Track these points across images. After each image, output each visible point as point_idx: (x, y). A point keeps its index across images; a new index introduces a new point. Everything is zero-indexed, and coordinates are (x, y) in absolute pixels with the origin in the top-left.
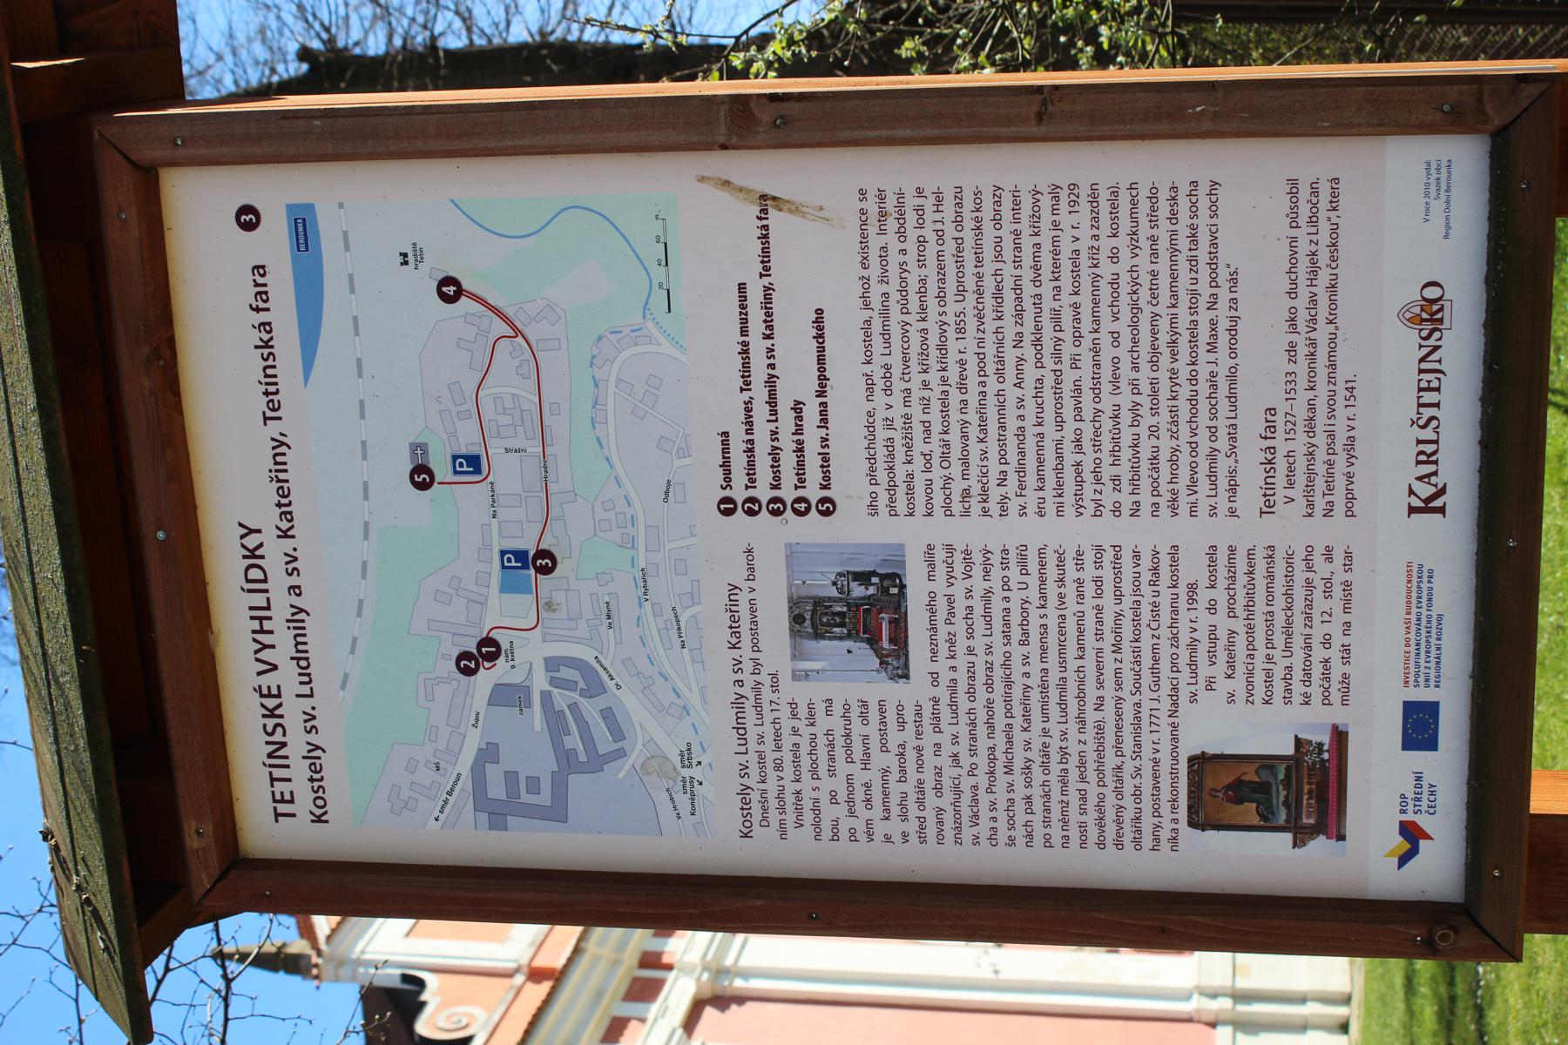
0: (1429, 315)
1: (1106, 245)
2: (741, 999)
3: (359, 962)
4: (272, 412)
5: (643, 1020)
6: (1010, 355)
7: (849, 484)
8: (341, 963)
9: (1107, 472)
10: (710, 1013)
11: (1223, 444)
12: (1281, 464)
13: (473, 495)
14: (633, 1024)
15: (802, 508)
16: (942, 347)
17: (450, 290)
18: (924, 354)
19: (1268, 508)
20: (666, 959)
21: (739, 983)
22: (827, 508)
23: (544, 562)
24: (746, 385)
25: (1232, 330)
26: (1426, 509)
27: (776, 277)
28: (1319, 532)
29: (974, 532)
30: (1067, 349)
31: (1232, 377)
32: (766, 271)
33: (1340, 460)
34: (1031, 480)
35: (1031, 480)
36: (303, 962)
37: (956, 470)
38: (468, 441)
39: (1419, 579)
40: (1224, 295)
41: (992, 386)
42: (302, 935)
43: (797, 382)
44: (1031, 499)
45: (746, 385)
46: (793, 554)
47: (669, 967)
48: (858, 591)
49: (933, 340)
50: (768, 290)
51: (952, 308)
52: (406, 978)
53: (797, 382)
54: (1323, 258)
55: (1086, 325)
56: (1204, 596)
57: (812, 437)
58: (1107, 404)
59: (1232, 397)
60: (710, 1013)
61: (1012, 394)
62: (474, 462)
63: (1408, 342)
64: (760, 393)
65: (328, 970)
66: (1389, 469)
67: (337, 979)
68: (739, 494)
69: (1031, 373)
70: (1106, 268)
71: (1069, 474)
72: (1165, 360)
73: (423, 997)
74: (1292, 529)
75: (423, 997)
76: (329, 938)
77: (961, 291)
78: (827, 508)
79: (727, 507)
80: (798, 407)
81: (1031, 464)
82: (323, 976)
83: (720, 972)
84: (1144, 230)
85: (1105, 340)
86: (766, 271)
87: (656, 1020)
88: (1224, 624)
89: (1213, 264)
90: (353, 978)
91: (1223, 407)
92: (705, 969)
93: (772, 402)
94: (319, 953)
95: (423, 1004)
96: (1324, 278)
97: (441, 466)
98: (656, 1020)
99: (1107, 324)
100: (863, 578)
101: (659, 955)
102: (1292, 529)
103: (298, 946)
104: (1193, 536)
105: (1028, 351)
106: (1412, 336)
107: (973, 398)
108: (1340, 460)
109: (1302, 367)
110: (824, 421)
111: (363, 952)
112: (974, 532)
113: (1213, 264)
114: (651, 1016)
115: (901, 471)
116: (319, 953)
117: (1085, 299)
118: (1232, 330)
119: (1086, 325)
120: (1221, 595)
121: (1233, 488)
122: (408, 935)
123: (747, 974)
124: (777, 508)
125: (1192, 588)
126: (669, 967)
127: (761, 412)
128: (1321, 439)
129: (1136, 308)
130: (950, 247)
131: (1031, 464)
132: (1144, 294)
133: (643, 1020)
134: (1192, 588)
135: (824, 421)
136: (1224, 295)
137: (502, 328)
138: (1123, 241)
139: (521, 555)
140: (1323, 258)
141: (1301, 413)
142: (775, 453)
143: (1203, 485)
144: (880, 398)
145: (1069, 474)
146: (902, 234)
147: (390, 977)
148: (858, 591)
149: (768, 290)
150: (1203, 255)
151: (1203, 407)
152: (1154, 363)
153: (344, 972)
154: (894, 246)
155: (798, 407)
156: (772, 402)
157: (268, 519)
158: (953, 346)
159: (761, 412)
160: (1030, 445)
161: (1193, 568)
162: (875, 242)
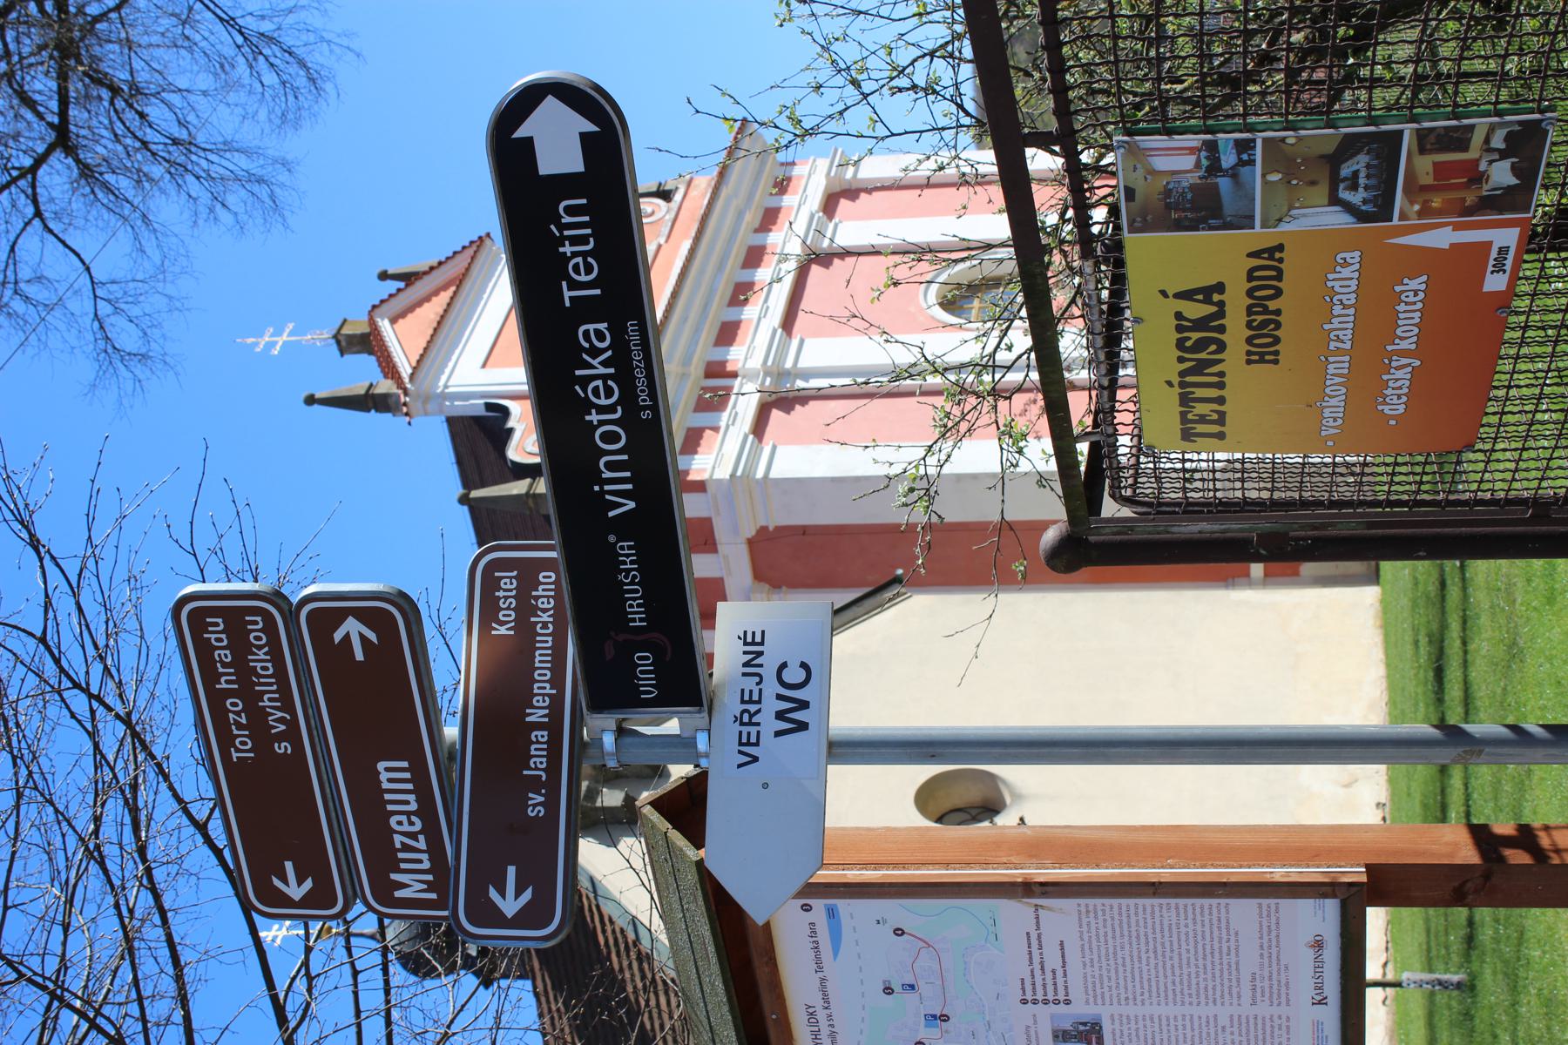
0: (1318, 945)
1: (1182, 922)
2: (803, 398)
3: (444, 396)
4: (819, 969)
5: (716, 429)
6: (1144, 957)
7: (1076, 993)
8: (427, 398)
9: (1186, 992)
10: (776, 414)
11: (1234, 983)
12: (1259, 990)
13: (911, 997)
14: (708, 433)
15: (1056, 1002)
16: (1115, 953)
17: (899, 932)
18: (1107, 955)
19: (1254, 1003)
20: (729, 368)
21: (800, 384)
22: (1068, 1002)
23: (945, 1018)
24: (1031, 963)
25: (1237, 950)
26: (1319, 1003)
27: (1042, 930)
28: (1275, 1010)
29: (1131, 1010)
30: (1168, 954)
31: (1237, 963)
32: (1038, 928)
33: (1283, 990)
34: (1154, 994)
35: (1154, 994)
36: (391, 401)
37: (1122, 990)
38: (909, 980)
39: (1318, 1026)
40: (1233, 938)
41: (1137, 965)
42: (386, 376)
43: (1053, 961)
44: (1155, 1000)
45: (1031, 963)
46: (1053, 1017)
47: (734, 375)
48: (1082, 1028)
49: (1111, 950)
50: (1039, 936)
51: (1118, 941)
52: (489, 407)
53: (1053, 961)
54: (1273, 927)
55: (1176, 946)
56: (1228, 1030)
57: (1060, 981)
58: (1185, 971)
59: (1237, 969)
60: (776, 414)
61: (1145, 968)
62: (912, 987)
63: (1311, 953)
64: (1037, 967)
65: (416, 407)
66: (1304, 988)
67: (426, 414)
68: (1029, 997)
69: (1152, 961)
70: (1183, 930)
71: (1170, 993)
72: (1209, 957)
73: (510, 424)
74: (1264, 1009)
75: (510, 424)
76: (412, 376)
77: (1122, 936)
78: (1068, 1002)
79: (1024, 1002)
80: (1054, 971)
81: (1154, 989)
82: (413, 412)
83: (781, 375)
84: (1199, 918)
85: (1184, 952)
86: (1038, 928)
87: (728, 427)
88: (1237, 1039)
89: (1228, 929)
90: (441, 412)
91: (1234, 973)
92: (767, 374)
93: (1042, 969)
94: (406, 393)
95: (511, 430)
96: (1274, 934)
97: (897, 987)
98: (728, 427)
99: (1184, 946)
100: (1085, 1024)
101: (723, 363)
102: (1264, 1009)
103: (385, 386)
104: (1224, 1013)
105: (1151, 954)
106: (1311, 952)
107: (1129, 969)
108: (1283, 990)
109: (1266, 960)
110: (1065, 975)
111: (446, 386)
112: (1131, 1010)
113: (1228, 929)
114: (723, 424)
115: (1099, 991)
116: (406, 393)
117: (1175, 938)
118: (1237, 950)
119: (1176, 946)
120: (1236, 1030)
121: (1239, 997)
122: (484, 366)
123: (807, 375)
124: (1046, 1002)
125: (1224, 1028)
126: (734, 375)
127: (1038, 972)
128: (1275, 982)
129: (1196, 942)
130: (1117, 922)
131: (1154, 989)
132: (1199, 938)
133: (716, 429)
134: (1224, 1028)
135: (1065, 975)
136: (1233, 938)
137: (922, 944)
138: (1190, 921)
139: (934, 1017)
140: (1273, 927)
141: (1266, 974)
142: (1044, 985)
143: (1227, 996)
144: (1089, 969)
145: (1170, 993)
146: (1096, 917)
147: (476, 407)
148: (1082, 1028)
149: (1039, 936)
150: (1223, 925)
151: (1226, 973)
152: (1204, 958)
153: (431, 407)
154: (1093, 922)
155: (1054, 971)
156: (1042, 969)
157: (818, 1002)
158: (1120, 954)
159: (1038, 972)
160: (1153, 984)
161: (1224, 1020)
162: (1085, 921)
